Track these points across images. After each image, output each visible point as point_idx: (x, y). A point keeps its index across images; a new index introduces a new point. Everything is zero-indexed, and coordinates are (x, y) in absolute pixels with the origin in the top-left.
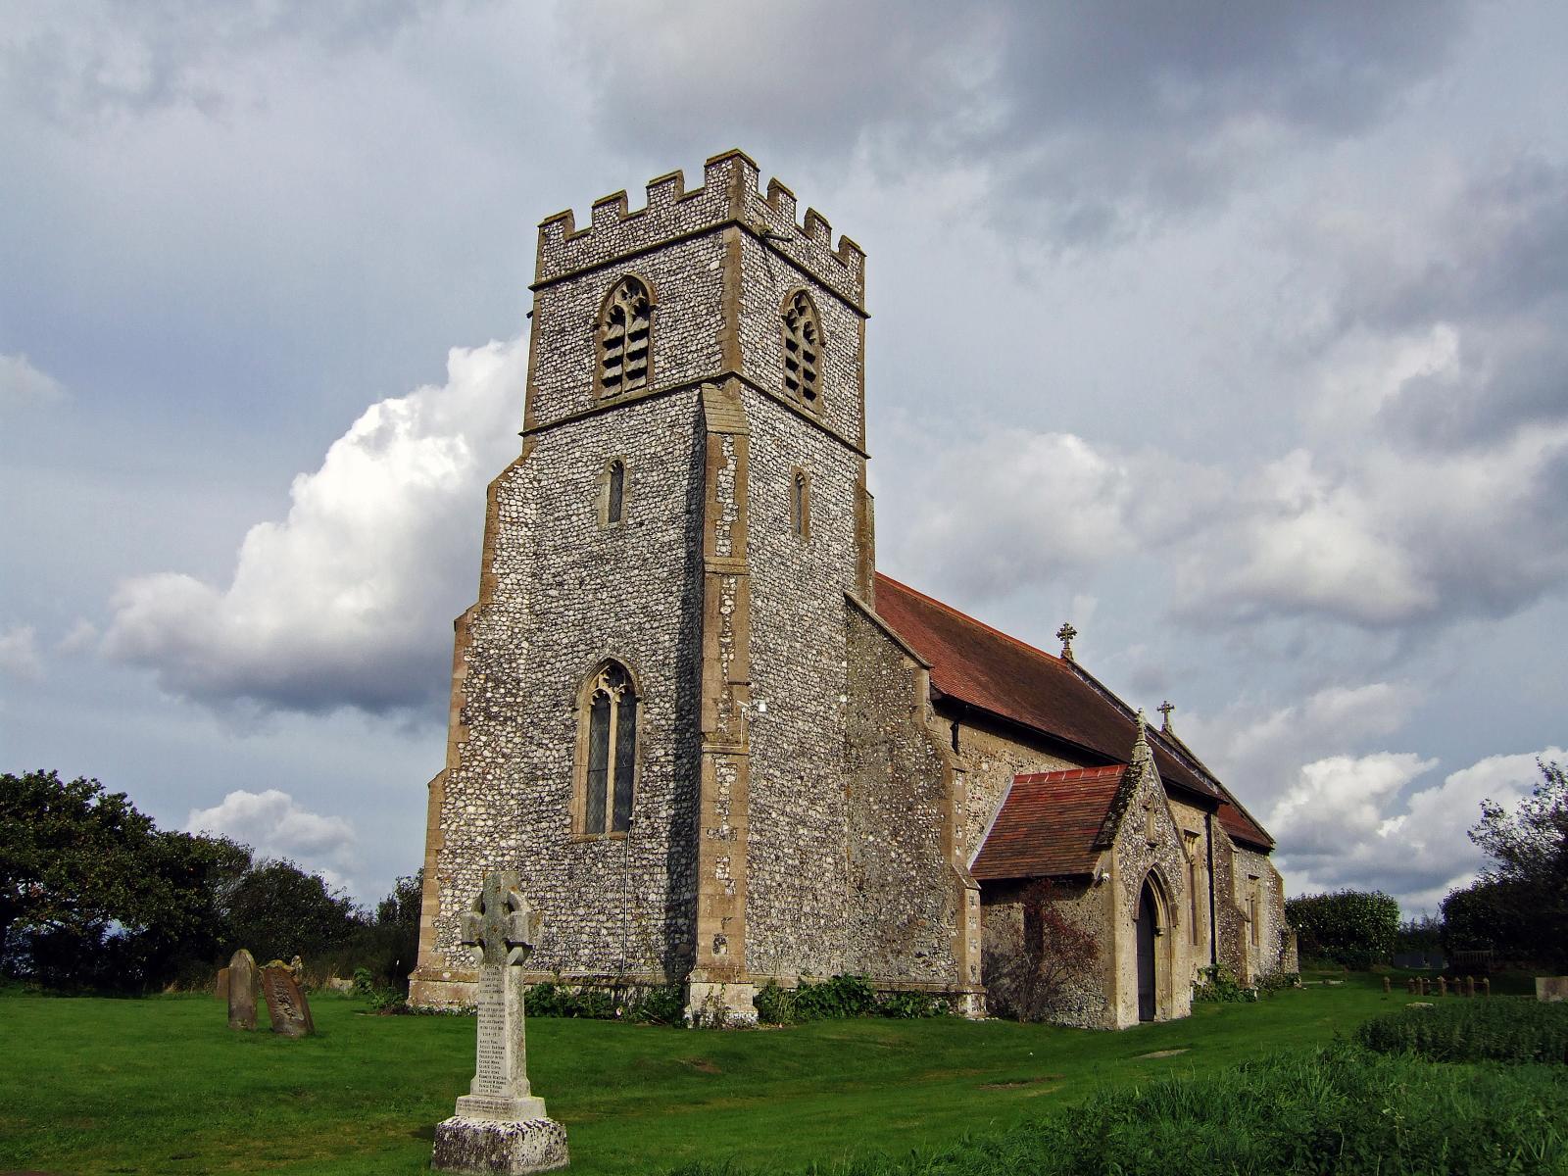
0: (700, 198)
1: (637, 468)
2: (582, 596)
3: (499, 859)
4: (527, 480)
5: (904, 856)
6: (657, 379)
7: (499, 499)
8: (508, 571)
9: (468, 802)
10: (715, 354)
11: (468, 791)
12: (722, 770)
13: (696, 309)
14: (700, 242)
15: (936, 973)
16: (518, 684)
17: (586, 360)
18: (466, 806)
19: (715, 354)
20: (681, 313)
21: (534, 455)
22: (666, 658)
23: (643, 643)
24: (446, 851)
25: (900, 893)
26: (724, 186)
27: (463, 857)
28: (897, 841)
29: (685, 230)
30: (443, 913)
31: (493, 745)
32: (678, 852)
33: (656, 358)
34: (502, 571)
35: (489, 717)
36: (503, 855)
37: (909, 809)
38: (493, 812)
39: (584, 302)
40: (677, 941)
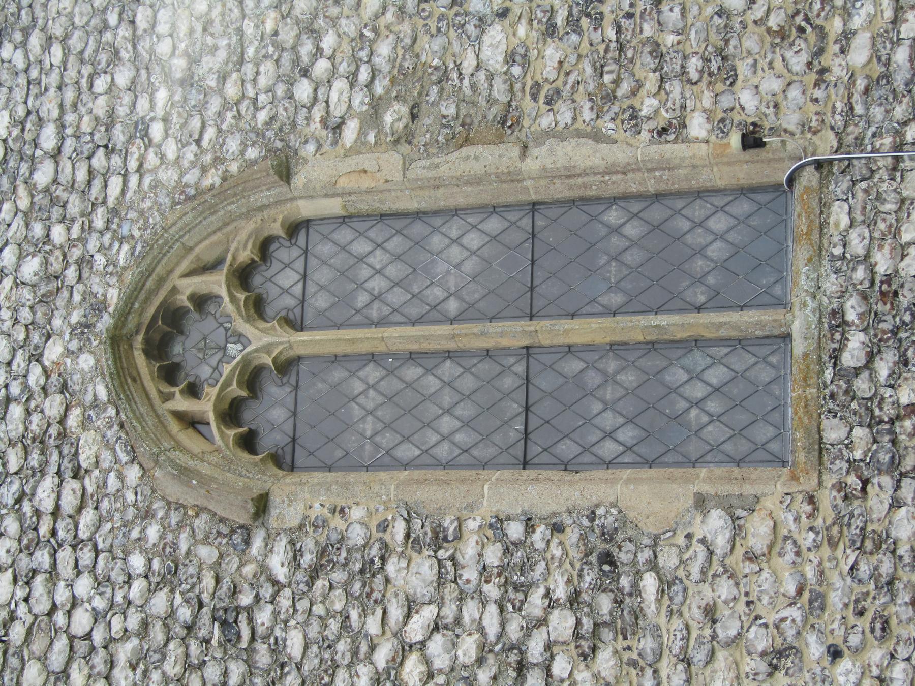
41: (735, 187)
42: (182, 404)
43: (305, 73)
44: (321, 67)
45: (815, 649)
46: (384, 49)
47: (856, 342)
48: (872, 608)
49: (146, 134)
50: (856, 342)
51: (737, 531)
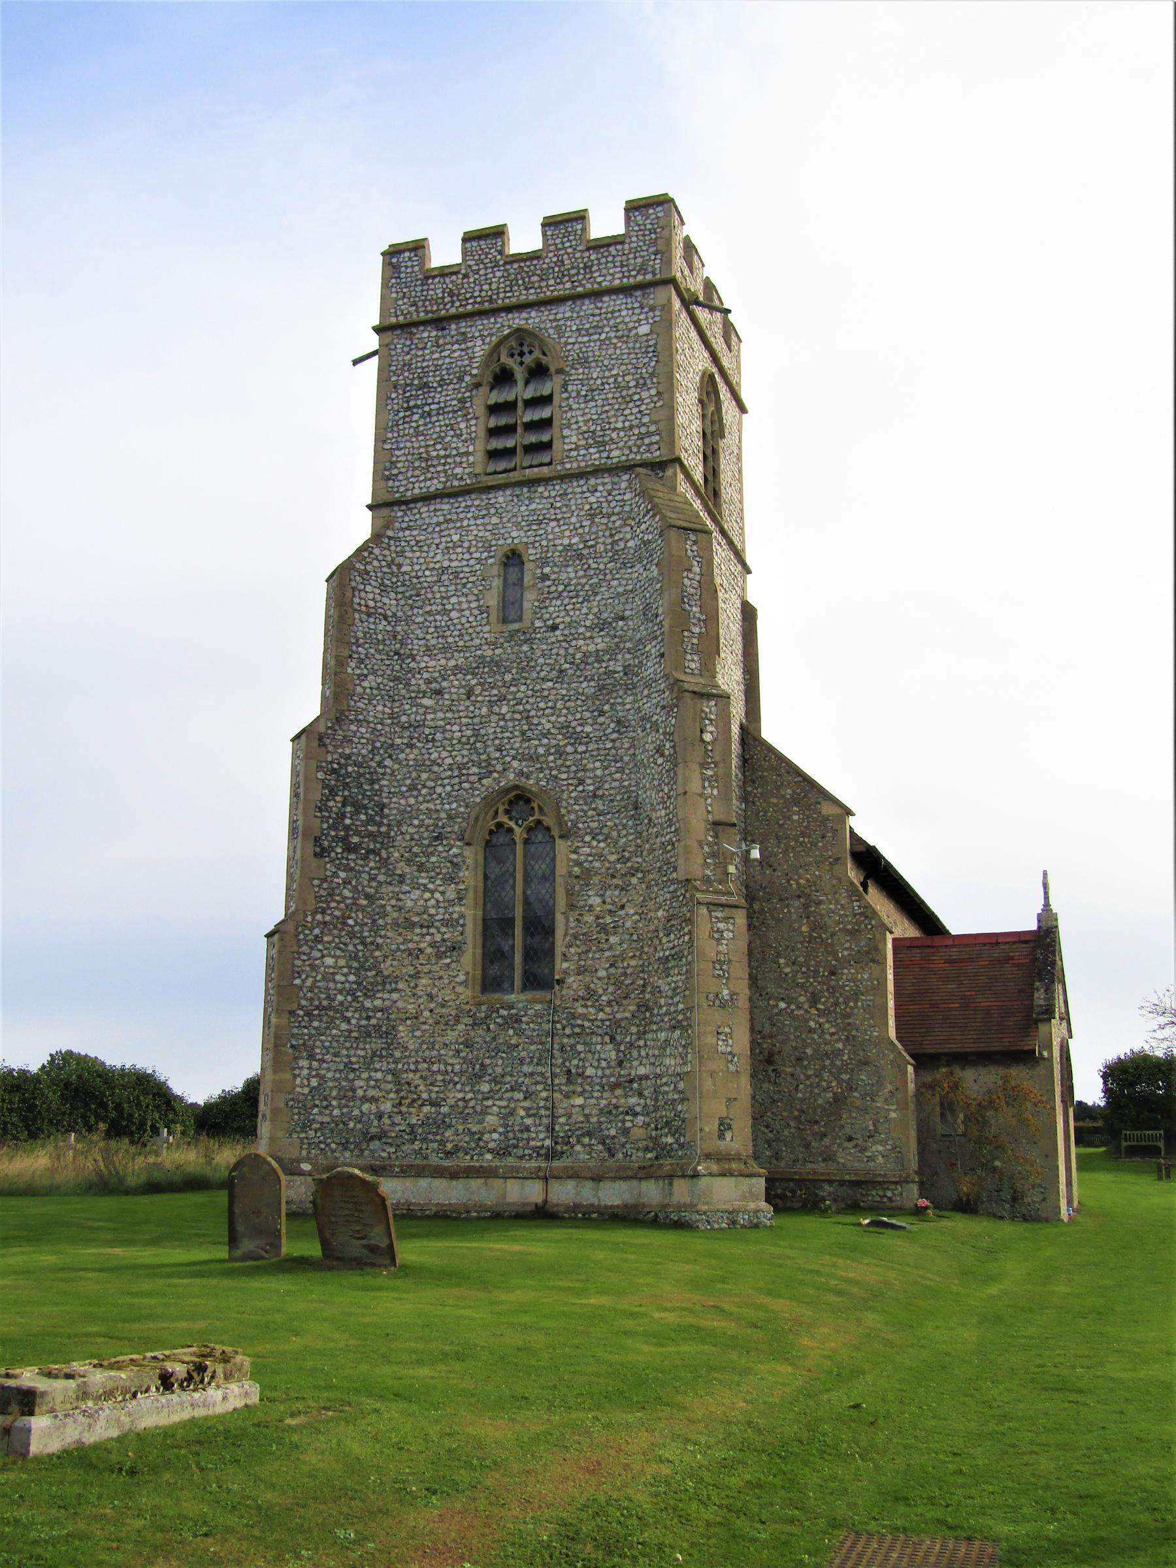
0: (619, 247)
1: (544, 562)
2: (472, 708)
3: (364, 1022)
4: (384, 563)
5: (827, 1026)
6: (568, 457)
7: (353, 584)
8: (365, 672)
9: (325, 952)
10: (649, 434)
11: (326, 939)
12: (719, 925)
13: (620, 379)
14: (620, 300)
15: (871, 1159)
16: (382, 810)
17: (463, 425)
18: (323, 956)
19: (649, 434)
20: (599, 382)
21: (390, 533)
22: (598, 789)
23: (563, 769)
24: (301, 1013)
25: (824, 1067)
26: (653, 236)
27: (321, 1021)
28: (818, 1010)
29: (599, 283)
30: (298, 1089)
31: (354, 883)
32: (626, 1018)
33: (566, 432)
34: (358, 672)
35: (350, 848)
36: (368, 1018)
37: (832, 973)
38: (355, 964)
39: (456, 355)
40: (629, 1124)
41: (369, 1269)
42: (501, 809)
43: (593, 838)
44: (594, 843)
45: (432, 1006)
46: (597, 864)
47: (505, 1013)
48: (442, 1020)
49: (580, 784)
50: (505, 1013)
51: (460, 984)
